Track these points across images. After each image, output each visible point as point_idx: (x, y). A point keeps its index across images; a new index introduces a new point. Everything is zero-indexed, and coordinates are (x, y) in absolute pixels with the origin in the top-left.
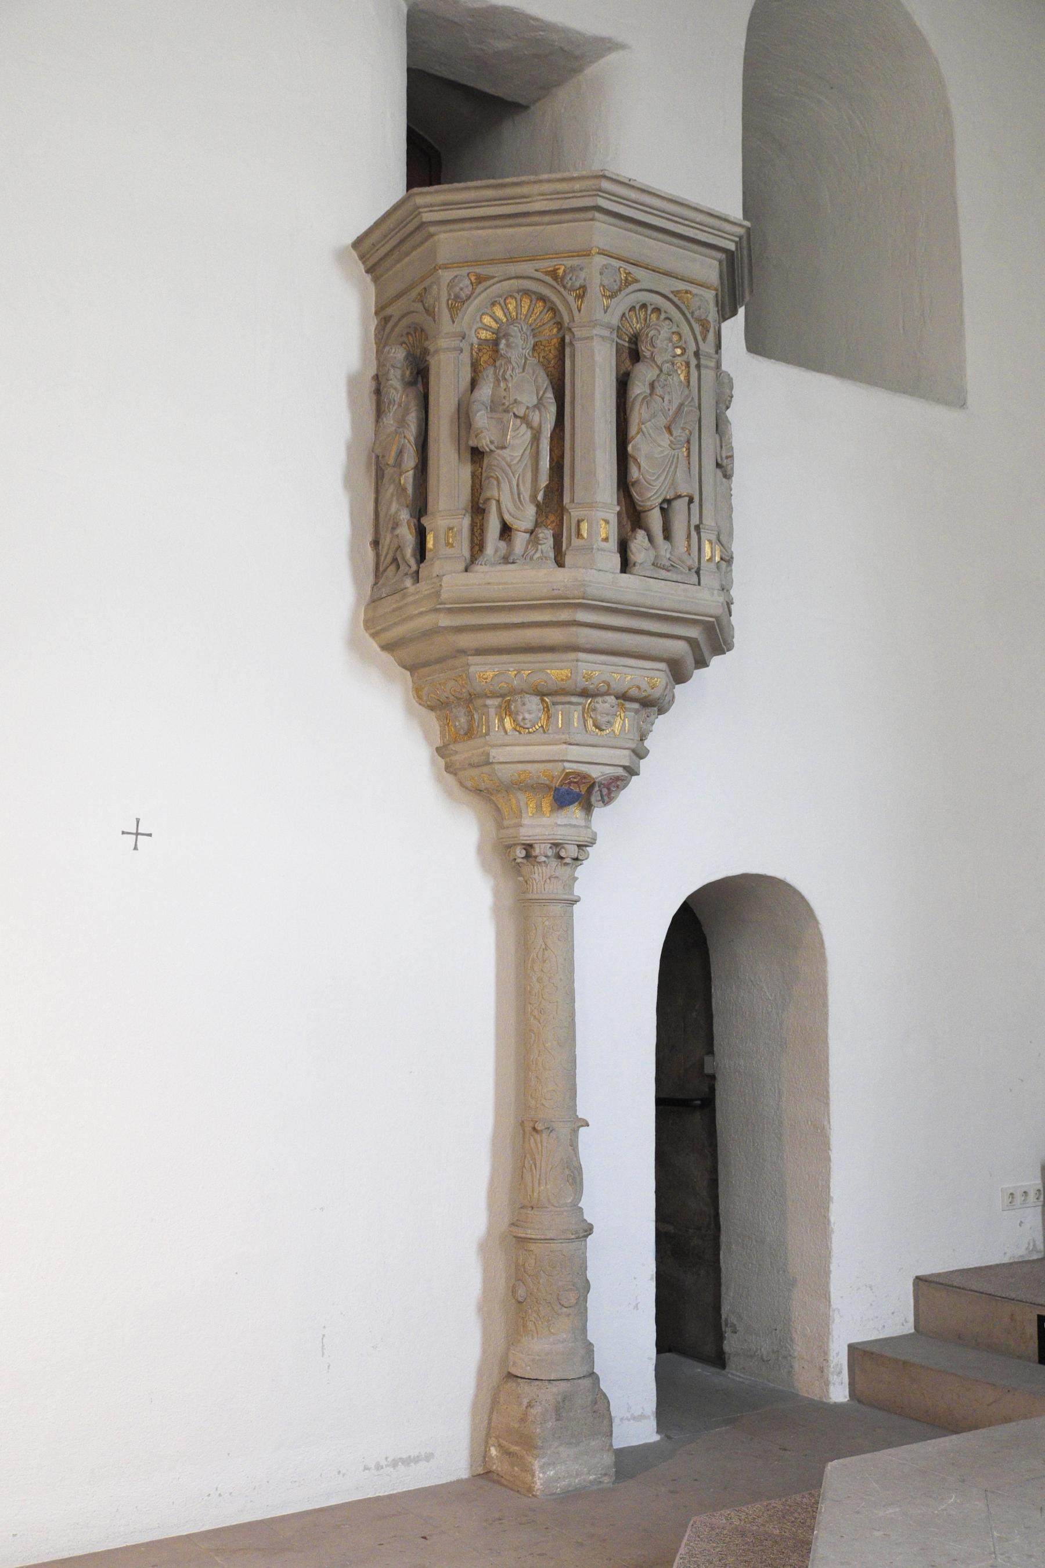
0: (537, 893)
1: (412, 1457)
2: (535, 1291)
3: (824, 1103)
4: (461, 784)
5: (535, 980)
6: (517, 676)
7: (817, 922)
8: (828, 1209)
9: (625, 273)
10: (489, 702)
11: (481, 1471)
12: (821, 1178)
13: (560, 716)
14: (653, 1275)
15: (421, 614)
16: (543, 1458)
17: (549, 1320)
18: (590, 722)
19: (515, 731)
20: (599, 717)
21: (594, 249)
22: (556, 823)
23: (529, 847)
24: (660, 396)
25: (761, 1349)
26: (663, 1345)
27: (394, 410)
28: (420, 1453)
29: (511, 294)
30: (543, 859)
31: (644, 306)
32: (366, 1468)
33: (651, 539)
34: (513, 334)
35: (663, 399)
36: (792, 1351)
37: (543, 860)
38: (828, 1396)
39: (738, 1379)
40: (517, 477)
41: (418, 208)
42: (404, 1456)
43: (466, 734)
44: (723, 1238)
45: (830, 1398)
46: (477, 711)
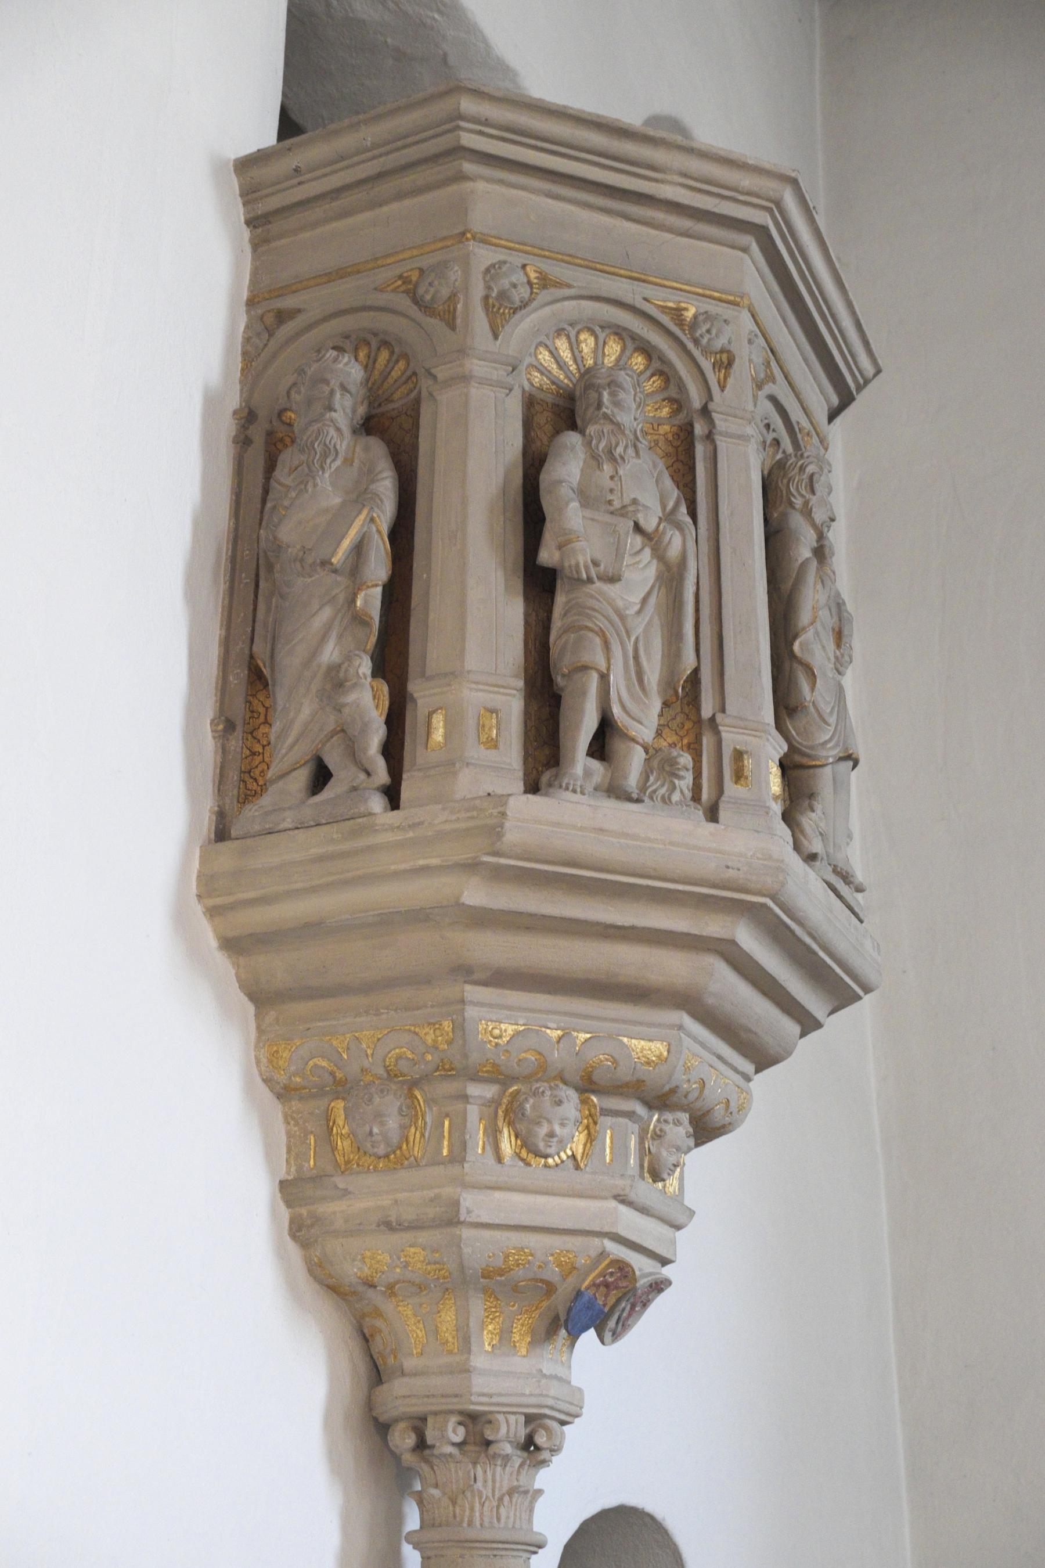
6: (562, 1041)
10: (474, 1090)
19: (517, 1159)
20: (664, 1153)
22: (541, 1371)
23: (472, 1419)
27: (333, 469)
29: (592, 326)
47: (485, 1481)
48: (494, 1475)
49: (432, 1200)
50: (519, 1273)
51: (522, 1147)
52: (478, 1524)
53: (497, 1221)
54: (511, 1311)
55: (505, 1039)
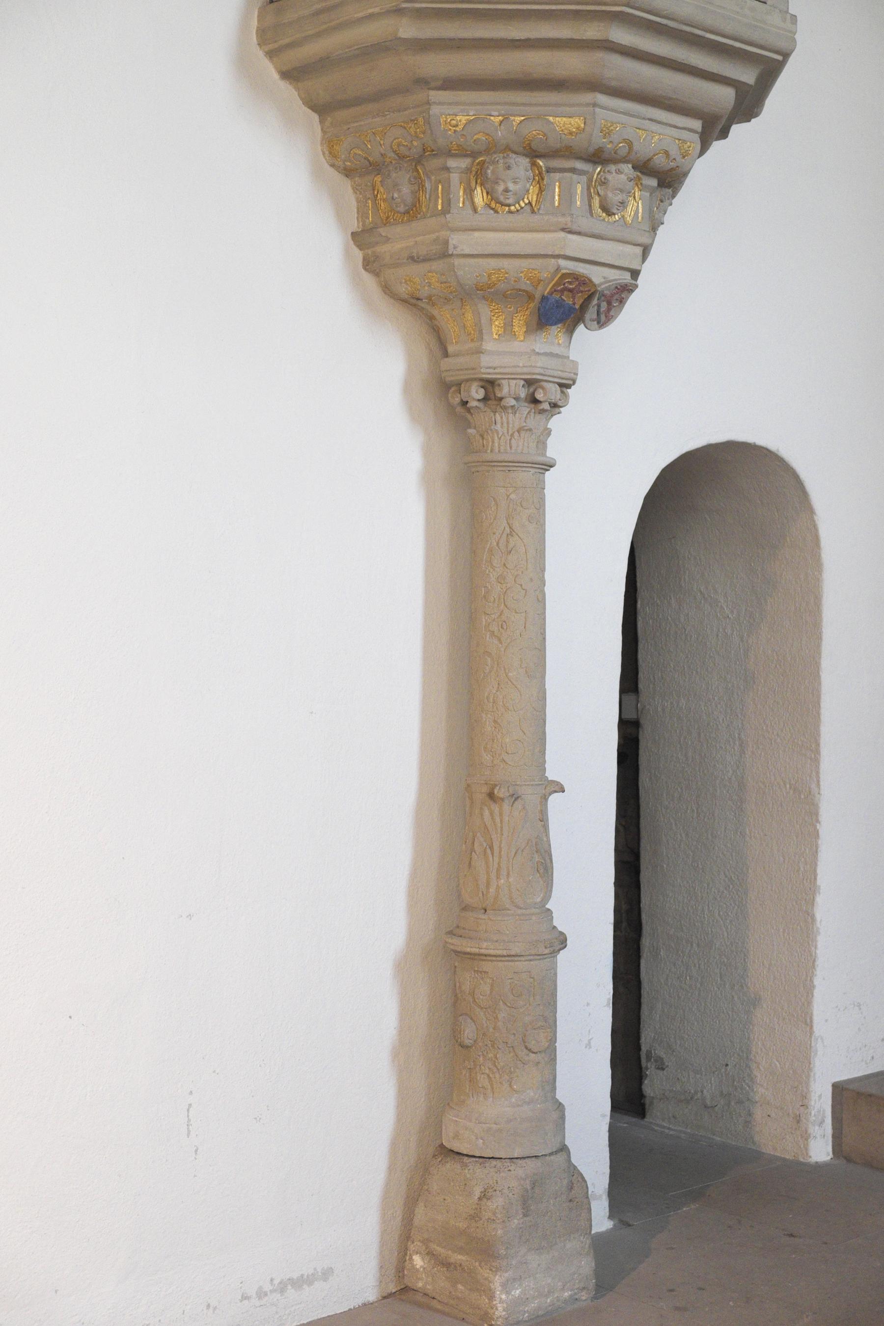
0: (499, 451)
1: (305, 1277)
2: (491, 1030)
3: (811, 759)
4: (387, 289)
5: (493, 579)
6: (502, 124)
7: (811, 511)
8: (812, 902)
10: (452, 163)
11: (392, 1288)
12: (803, 860)
13: (557, 190)
14: (609, 999)
15: (371, 17)
16: (506, 1272)
17: (511, 1072)
18: (596, 202)
19: (488, 209)
20: (610, 195)
22: (534, 350)
23: (490, 385)
25: (702, 1092)
28: (315, 1269)
30: (513, 402)
32: (245, 1297)
36: (752, 1094)
37: (512, 404)
38: (807, 1154)
39: (667, 1131)
42: (295, 1275)
43: (407, 212)
44: (646, 942)
45: (810, 1157)
46: (429, 178)
47: (502, 424)
48: (508, 419)
49: (435, 240)
50: (502, 286)
51: (492, 200)
52: (497, 450)
53: (476, 252)
54: (510, 311)
55: (461, 127)
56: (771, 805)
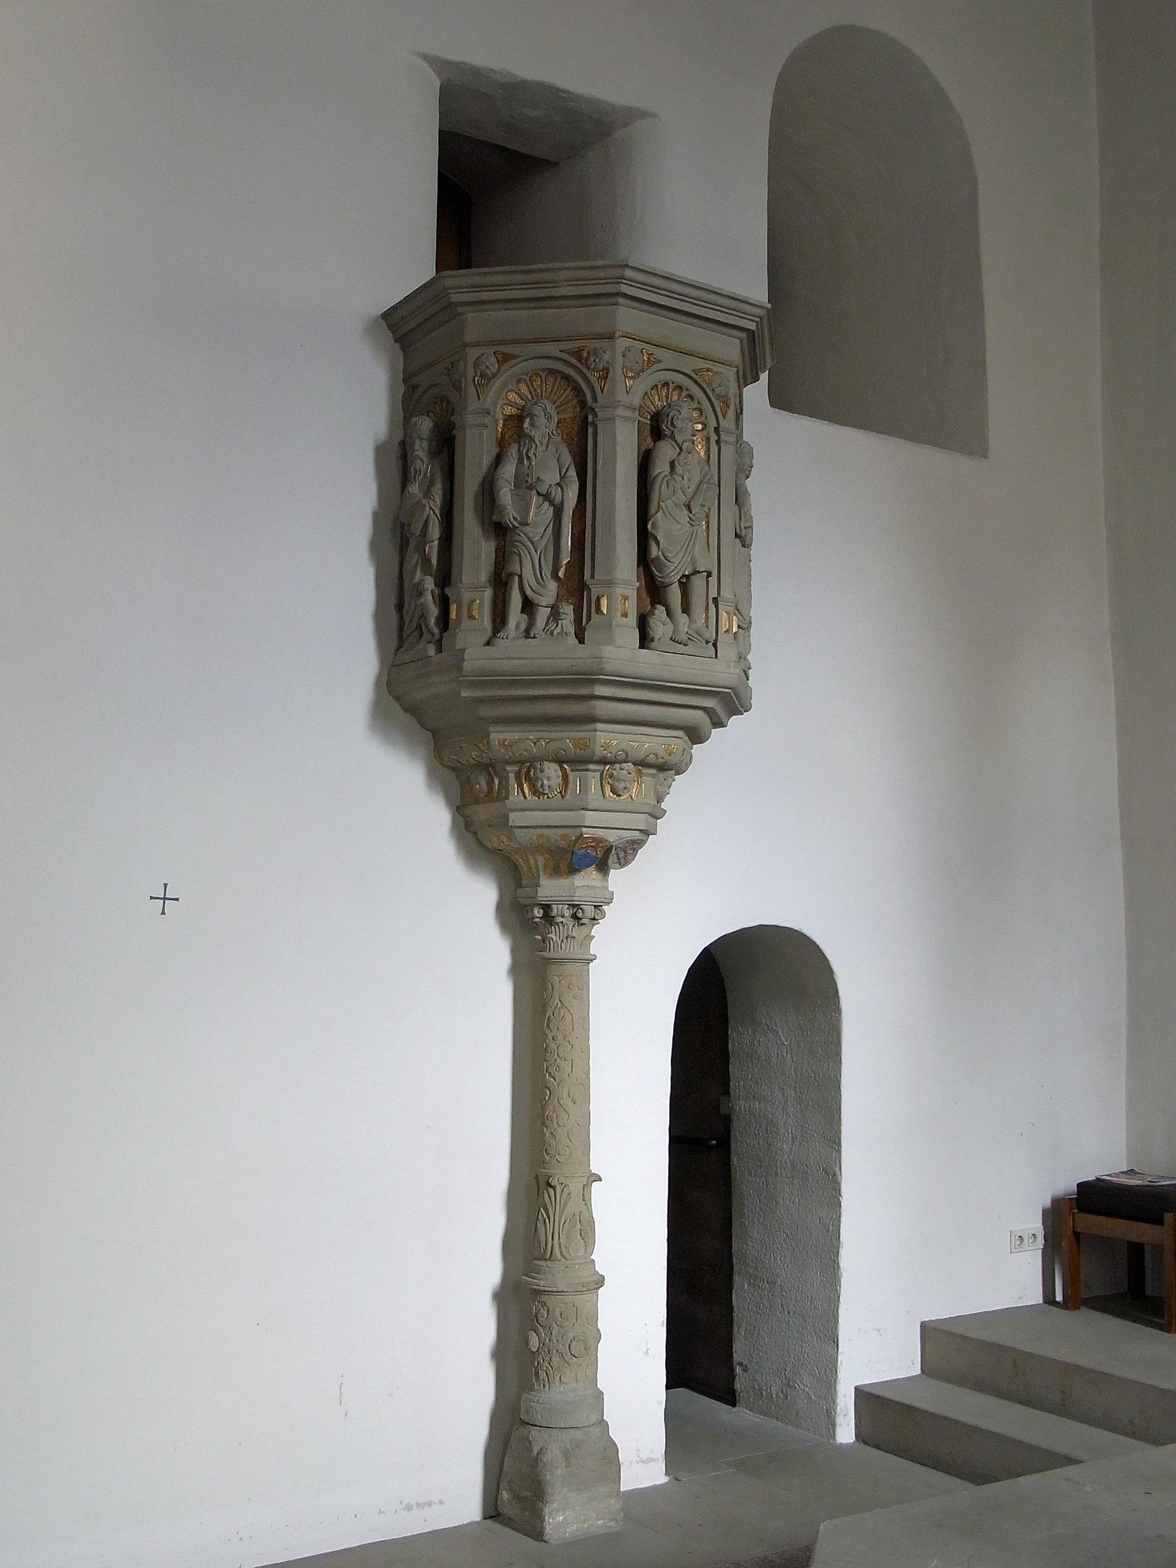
9: (648, 353)
14: (664, 1321)
18: (607, 789)
21: (618, 332)
23: (546, 908)
24: (680, 476)
26: (672, 1382)
31: (666, 384)
33: (669, 614)
34: (536, 413)
35: (683, 478)
40: (539, 553)
41: (447, 289)
56: (811, 1182)
